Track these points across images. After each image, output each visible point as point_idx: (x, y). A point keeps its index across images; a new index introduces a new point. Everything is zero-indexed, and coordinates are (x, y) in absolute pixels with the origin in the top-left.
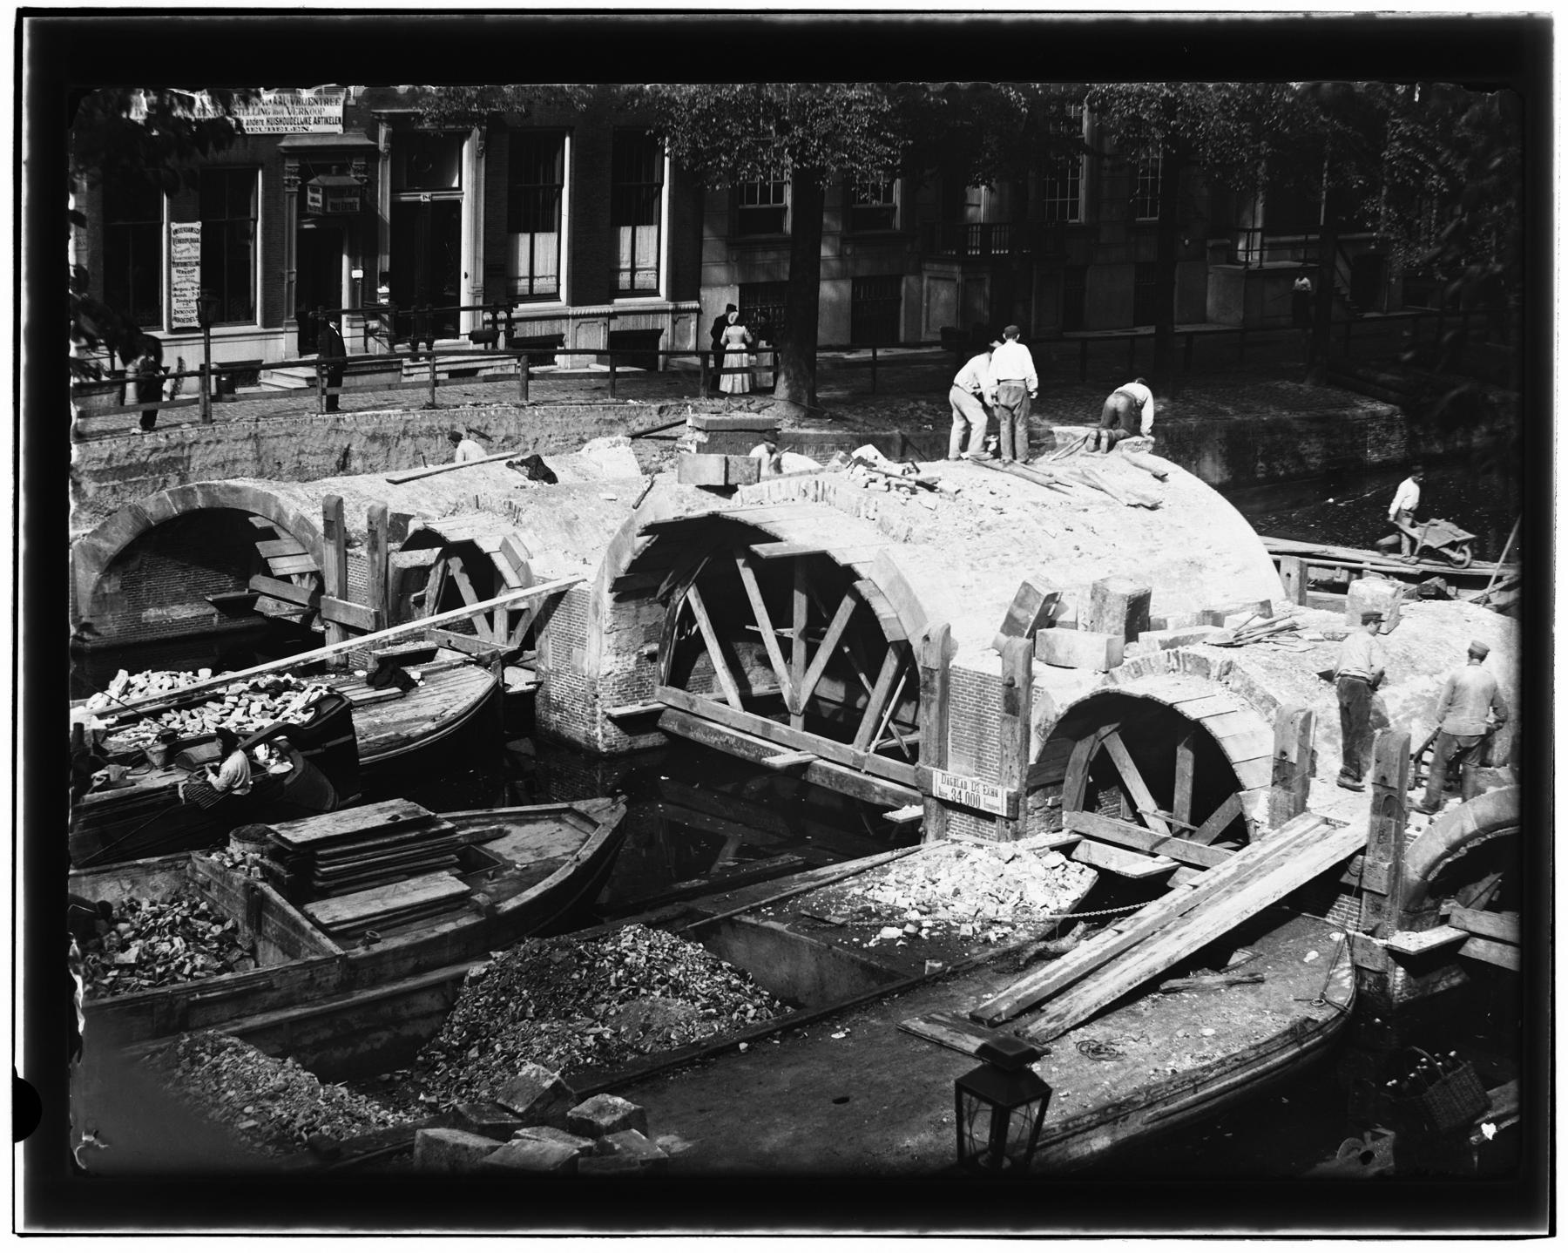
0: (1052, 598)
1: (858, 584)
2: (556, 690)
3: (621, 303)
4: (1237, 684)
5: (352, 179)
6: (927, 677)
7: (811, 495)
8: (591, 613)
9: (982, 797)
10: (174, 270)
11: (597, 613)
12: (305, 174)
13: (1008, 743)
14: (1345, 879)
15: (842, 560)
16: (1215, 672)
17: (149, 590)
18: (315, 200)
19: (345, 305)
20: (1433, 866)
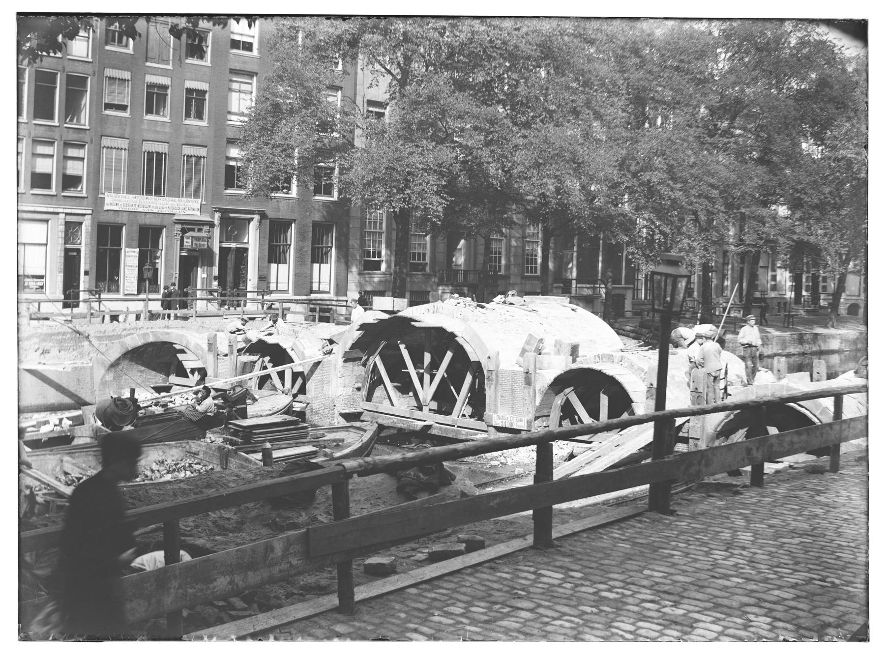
0: (541, 340)
1: (457, 338)
2: (315, 405)
3: (313, 296)
4: (626, 365)
5: (203, 234)
6: (489, 374)
7: (432, 311)
8: (332, 369)
9: (515, 422)
10: (126, 268)
11: (335, 369)
12: (184, 231)
13: (527, 398)
14: (681, 434)
15: (449, 330)
16: (616, 360)
17: (125, 381)
18: (188, 243)
19: (199, 286)
20: (719, 425)
